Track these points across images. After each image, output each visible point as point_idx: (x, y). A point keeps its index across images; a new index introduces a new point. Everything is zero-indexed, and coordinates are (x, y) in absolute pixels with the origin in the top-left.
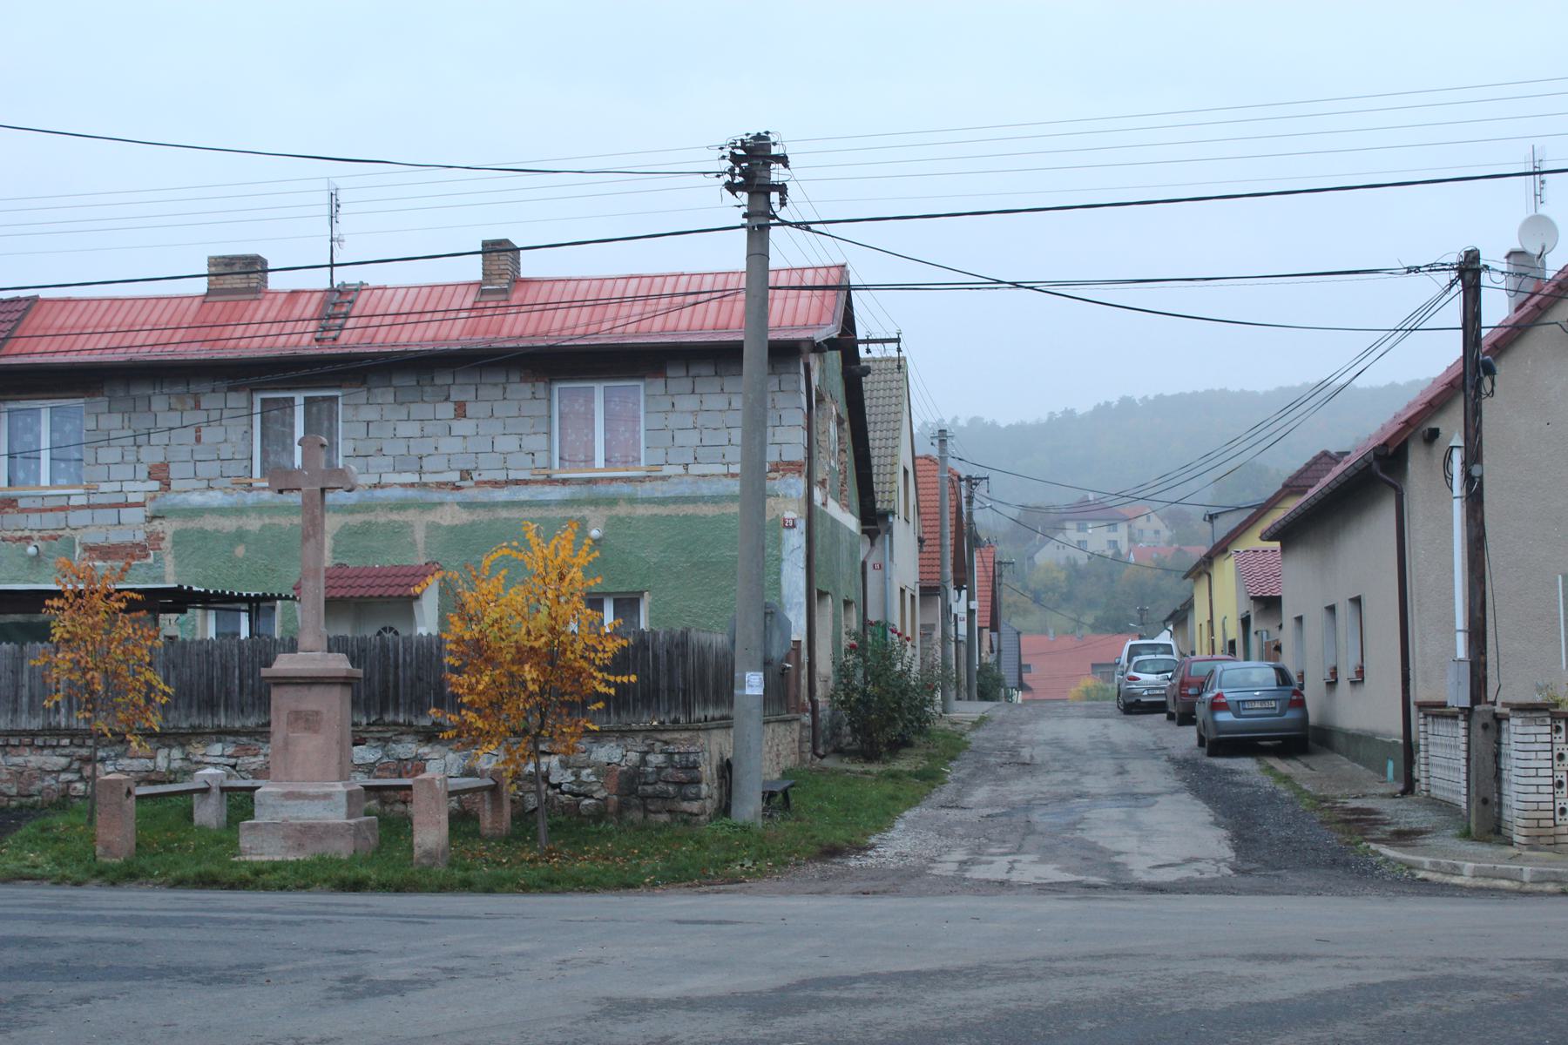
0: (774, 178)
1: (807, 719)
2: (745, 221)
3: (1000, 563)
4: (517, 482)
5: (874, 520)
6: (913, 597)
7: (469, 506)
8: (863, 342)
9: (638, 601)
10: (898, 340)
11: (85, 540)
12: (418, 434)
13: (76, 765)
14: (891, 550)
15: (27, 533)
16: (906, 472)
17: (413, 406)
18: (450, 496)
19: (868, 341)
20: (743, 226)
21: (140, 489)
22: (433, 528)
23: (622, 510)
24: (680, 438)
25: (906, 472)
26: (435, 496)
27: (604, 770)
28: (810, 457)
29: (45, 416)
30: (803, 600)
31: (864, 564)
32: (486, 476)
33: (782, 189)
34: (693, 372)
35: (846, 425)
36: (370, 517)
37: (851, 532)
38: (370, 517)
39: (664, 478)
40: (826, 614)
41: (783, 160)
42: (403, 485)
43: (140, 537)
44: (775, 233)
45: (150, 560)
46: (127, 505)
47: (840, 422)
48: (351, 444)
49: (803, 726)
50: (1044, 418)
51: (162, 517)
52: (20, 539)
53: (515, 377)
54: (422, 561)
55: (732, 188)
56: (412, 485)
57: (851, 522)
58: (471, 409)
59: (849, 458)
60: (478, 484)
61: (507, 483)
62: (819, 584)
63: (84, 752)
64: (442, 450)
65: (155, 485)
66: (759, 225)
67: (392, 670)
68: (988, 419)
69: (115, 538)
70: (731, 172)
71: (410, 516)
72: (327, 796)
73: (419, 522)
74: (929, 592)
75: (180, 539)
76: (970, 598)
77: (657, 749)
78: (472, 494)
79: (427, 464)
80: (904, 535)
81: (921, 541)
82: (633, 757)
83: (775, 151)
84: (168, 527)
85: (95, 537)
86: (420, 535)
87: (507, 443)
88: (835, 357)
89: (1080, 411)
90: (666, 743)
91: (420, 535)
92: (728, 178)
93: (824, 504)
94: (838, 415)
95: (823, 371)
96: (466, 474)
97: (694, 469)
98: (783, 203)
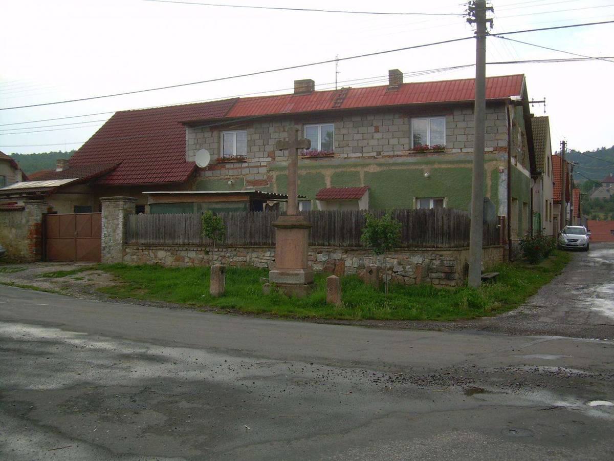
0: (487, 17)
1: (507, 247)
2: (476, 35)
3: (581, 195)
4: (397, 156)
5: (536, 174)
6: (550, 204)
7: (380, 165)
8: (531, 102)
9: (442, 200)
10: (544, 102)
11: (248, 179)
12: (361, 138)
13: (220, 259)
14: (543, 186)
15: (228, 177)
16: (548, 158)
17: (359, 128)
18: (372, 161)
19: (533, 102)
20: (474, 37)
21: (265, 161)
22: (366, 173)
23: (436, 166)
24: (459, 138)
25: (548, 158)
26: (368, 161)
27: (417, 266)
28: (509, 145)
29: (235, 136)
30: (506, 200)
31: (532, 189)
32: (386, 154)
33: (491, 21)
34: (464, 113)
35: (525, 136)
36: (344, 170)
37: (526, 177)
38: (344, 170)
39: (453, 153)
40: (516, 207)
41: (491, 9)
42: (356, 157)
43: (265, 177)
44: (488, 39)
45: (268, 186)
46: (261, 166)
47: (522, 135)
48: (337, 143)
49: (505, 250)
50: (596, 150)
51: (273, 170)
52: (226, 179)
53: (397, 116)
54: (363, 186)
55: (470, 21)
56: (359, 157)
57: (527, 173)
58: (380, 129)
59: (526, 149)
60: (383, 157)
61: (394, 156)
62: (513, 195)
63: (223, 254)
64: (370, 144)
65: (270, 159)
66: (481, 36)
67: (333, 224)
68: (577, 151)
69: (257, 178)
70: (469, 14)
71: (359, 169)
72: (297, 275)
73: (362, 171)
74: (556, 203)
75: (278, 178)
76: (571, 205)
77: (438, 259)
78: (382, 161)
79: (365, 150)
80: (547, 180)
81: (554, 184)
82: (427, 261)
83: (487, 6)
84: (274, 174)
85: (250, 178)
86: (362, 176)
87: (393, 141)
88: (520, 108)
89: (607, 148)
90: (441, 256)
91: (362, 176)
92: (467, 17)
93: (516, 165)
94: (522, 132)
95: (515, 114)
96: (379, 153)
97: (464, 150)
98: (491, 27)
